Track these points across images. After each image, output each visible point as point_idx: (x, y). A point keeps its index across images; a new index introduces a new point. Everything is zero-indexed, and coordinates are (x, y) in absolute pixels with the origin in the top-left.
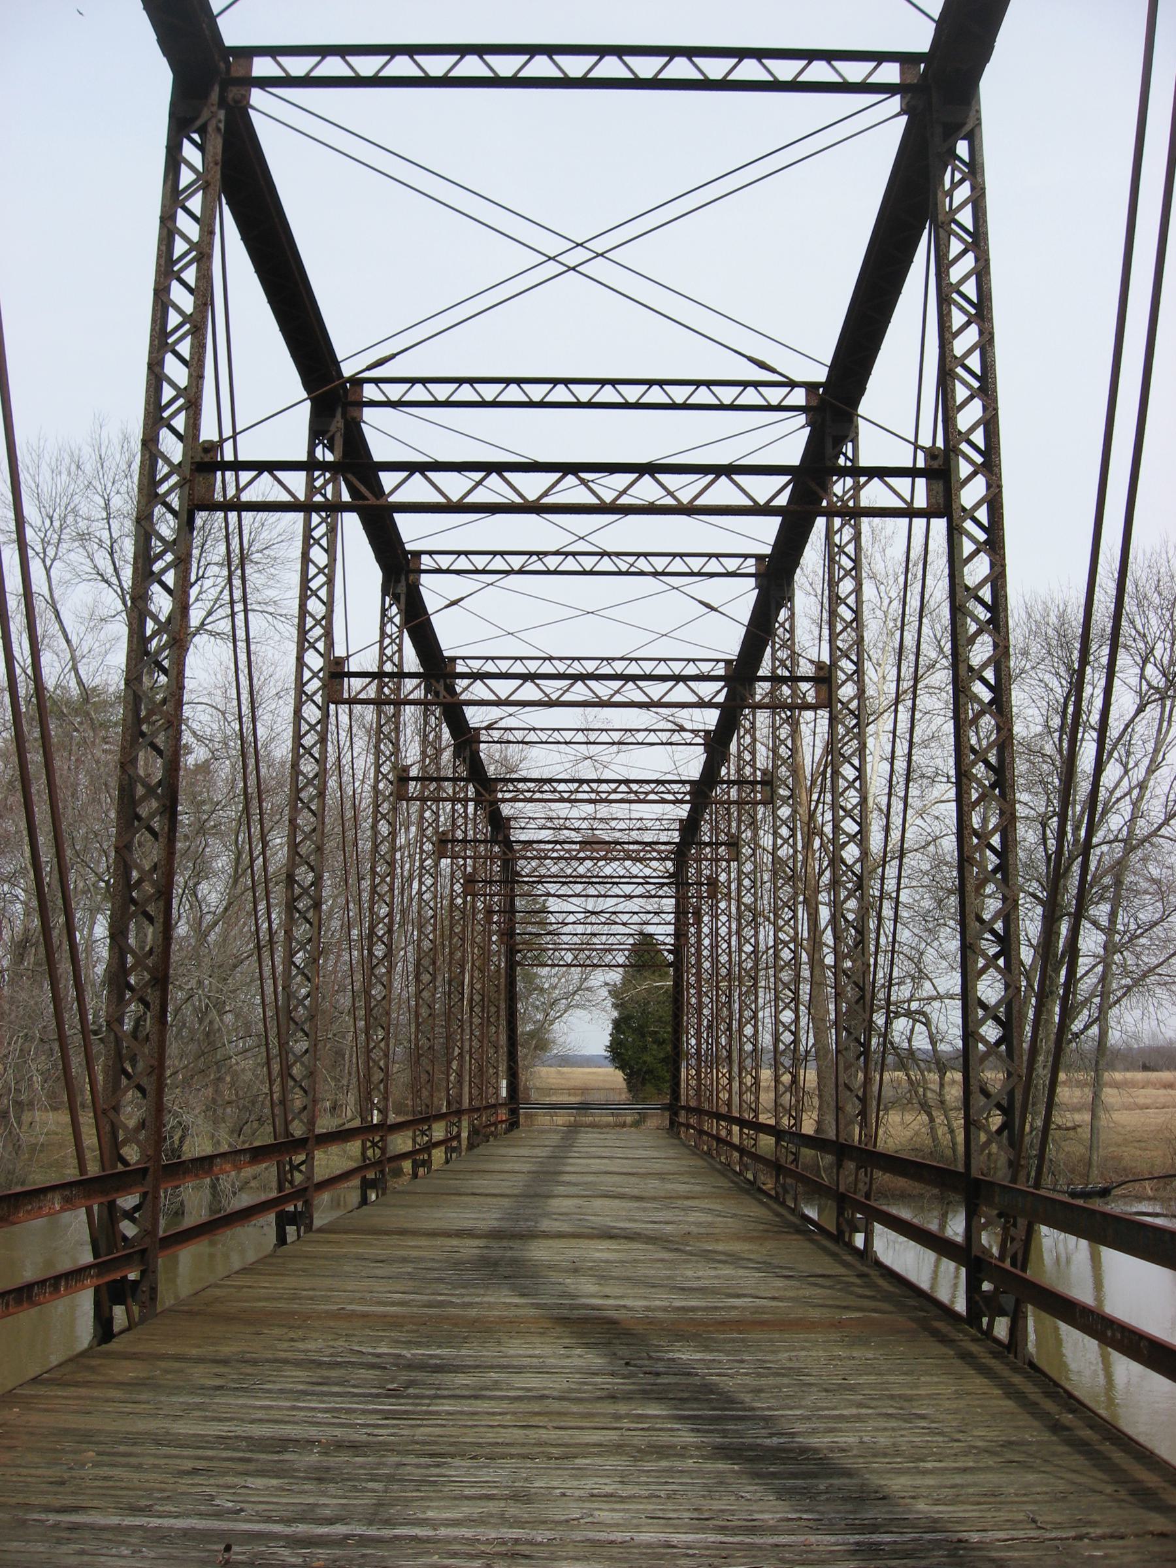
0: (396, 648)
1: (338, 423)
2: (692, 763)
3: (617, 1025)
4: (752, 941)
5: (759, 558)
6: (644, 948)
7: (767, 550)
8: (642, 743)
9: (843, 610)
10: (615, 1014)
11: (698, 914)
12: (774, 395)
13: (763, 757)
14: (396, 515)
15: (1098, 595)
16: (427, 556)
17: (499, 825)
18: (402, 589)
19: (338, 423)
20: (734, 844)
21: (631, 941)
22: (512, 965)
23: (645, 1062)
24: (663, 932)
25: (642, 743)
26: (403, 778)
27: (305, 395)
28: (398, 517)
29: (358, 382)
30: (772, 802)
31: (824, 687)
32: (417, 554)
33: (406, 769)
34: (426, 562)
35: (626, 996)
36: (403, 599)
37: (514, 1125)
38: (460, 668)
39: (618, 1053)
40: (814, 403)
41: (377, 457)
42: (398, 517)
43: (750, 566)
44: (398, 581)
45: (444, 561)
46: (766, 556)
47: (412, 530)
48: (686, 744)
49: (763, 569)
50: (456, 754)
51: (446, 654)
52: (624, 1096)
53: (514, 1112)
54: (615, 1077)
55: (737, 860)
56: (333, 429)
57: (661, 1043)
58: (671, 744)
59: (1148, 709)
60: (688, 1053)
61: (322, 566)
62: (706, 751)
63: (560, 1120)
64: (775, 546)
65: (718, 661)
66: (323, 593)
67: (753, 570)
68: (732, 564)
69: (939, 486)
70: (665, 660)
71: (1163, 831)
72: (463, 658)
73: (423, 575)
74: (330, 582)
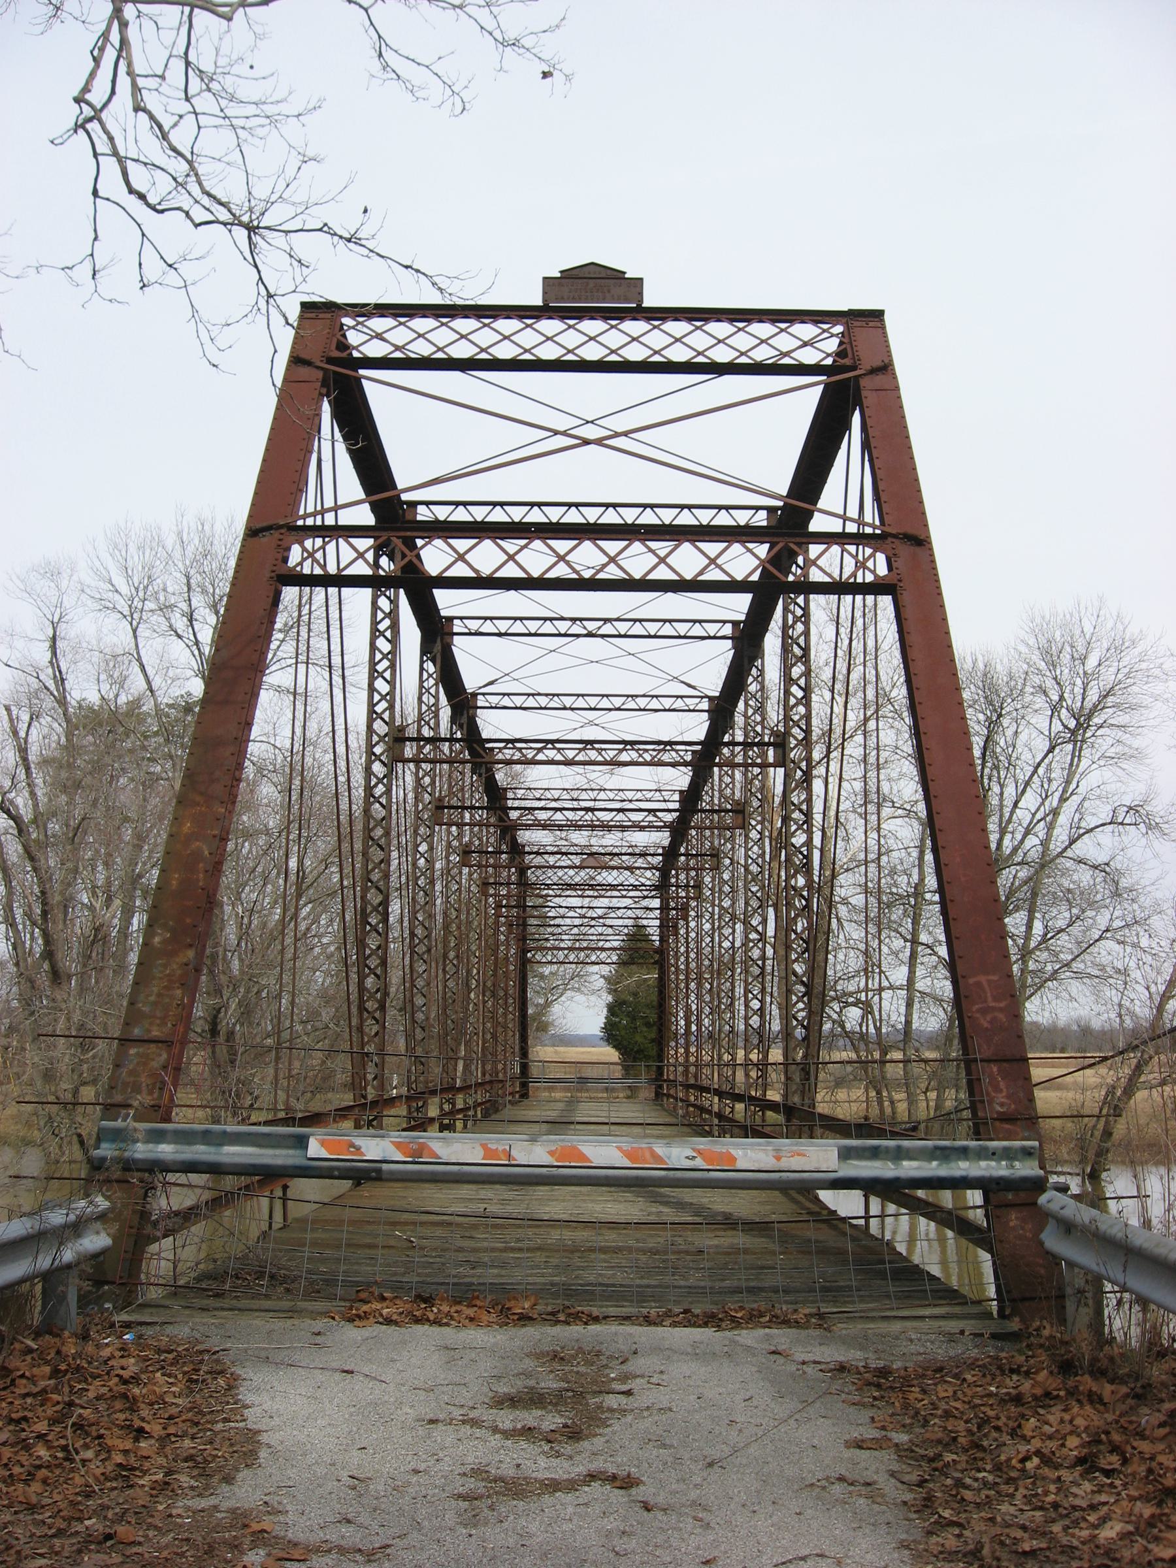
0: (425, 684)
1: (438, 647)
2: (697, 728)
3: (612, 1009)
4: (730, 938)
5: (735, 624)
6: (637, 935)
7: (743, 618)
8: (644, 710)
9: (794, 689)
10: (610, 998)
11: (676, 927)
12: (691, 702)
13: (774, 714)
14: (435, 591)
15: (466, 1191)
16: (424, 507)
17: (496, 796)
18: (464, 720)
19: (438, 647)
20: (715, 855)
21: (626, 931)
22: (524, 965)
23: (636, 1043)
24: (653, 925)
25: (644, 710)
26: (398, 737)
27: (362, 496)
28: (437, 593)
29: (475, 695)
30: (718, 868)
31: (740, 816)
32: (450, 619)
33: (402, 729)
34: (458, 627)
35: (620, 987)
36: (465, 727)
37: (525, 1095)
38: (527, 849)
39: (612, 1033)
40: (737, 635)
41: (484, 736)
42: (437, 593)
43: (728, 630)
44: (462, 715)
45: (474, 625)
46: (740, 622)
47: (447, 601)
48: (690, 710)
49: (713, 706)
50: (453, 720)
51: (443, 613)
52: (618, 1072)
53: (524, 1085)
54: (611, 1054)
55: (743, 828)
56: (435, 650)
57: (648, 1025)
58: (674, 710)
59: (1057, 750)
60: (676, 1034)
61: (385, 652)
62: (734, 647)
63: (558, 1095)
64: (748, 614)
65: (725, 622)
66: (387, 675)
67: (706, 708)
68: (712, 629)
69: (780, 751)
70: (670, 621)
71: (1069, 853)
72: (461, 618)
73: (455, 637)
74: (392, 666)
